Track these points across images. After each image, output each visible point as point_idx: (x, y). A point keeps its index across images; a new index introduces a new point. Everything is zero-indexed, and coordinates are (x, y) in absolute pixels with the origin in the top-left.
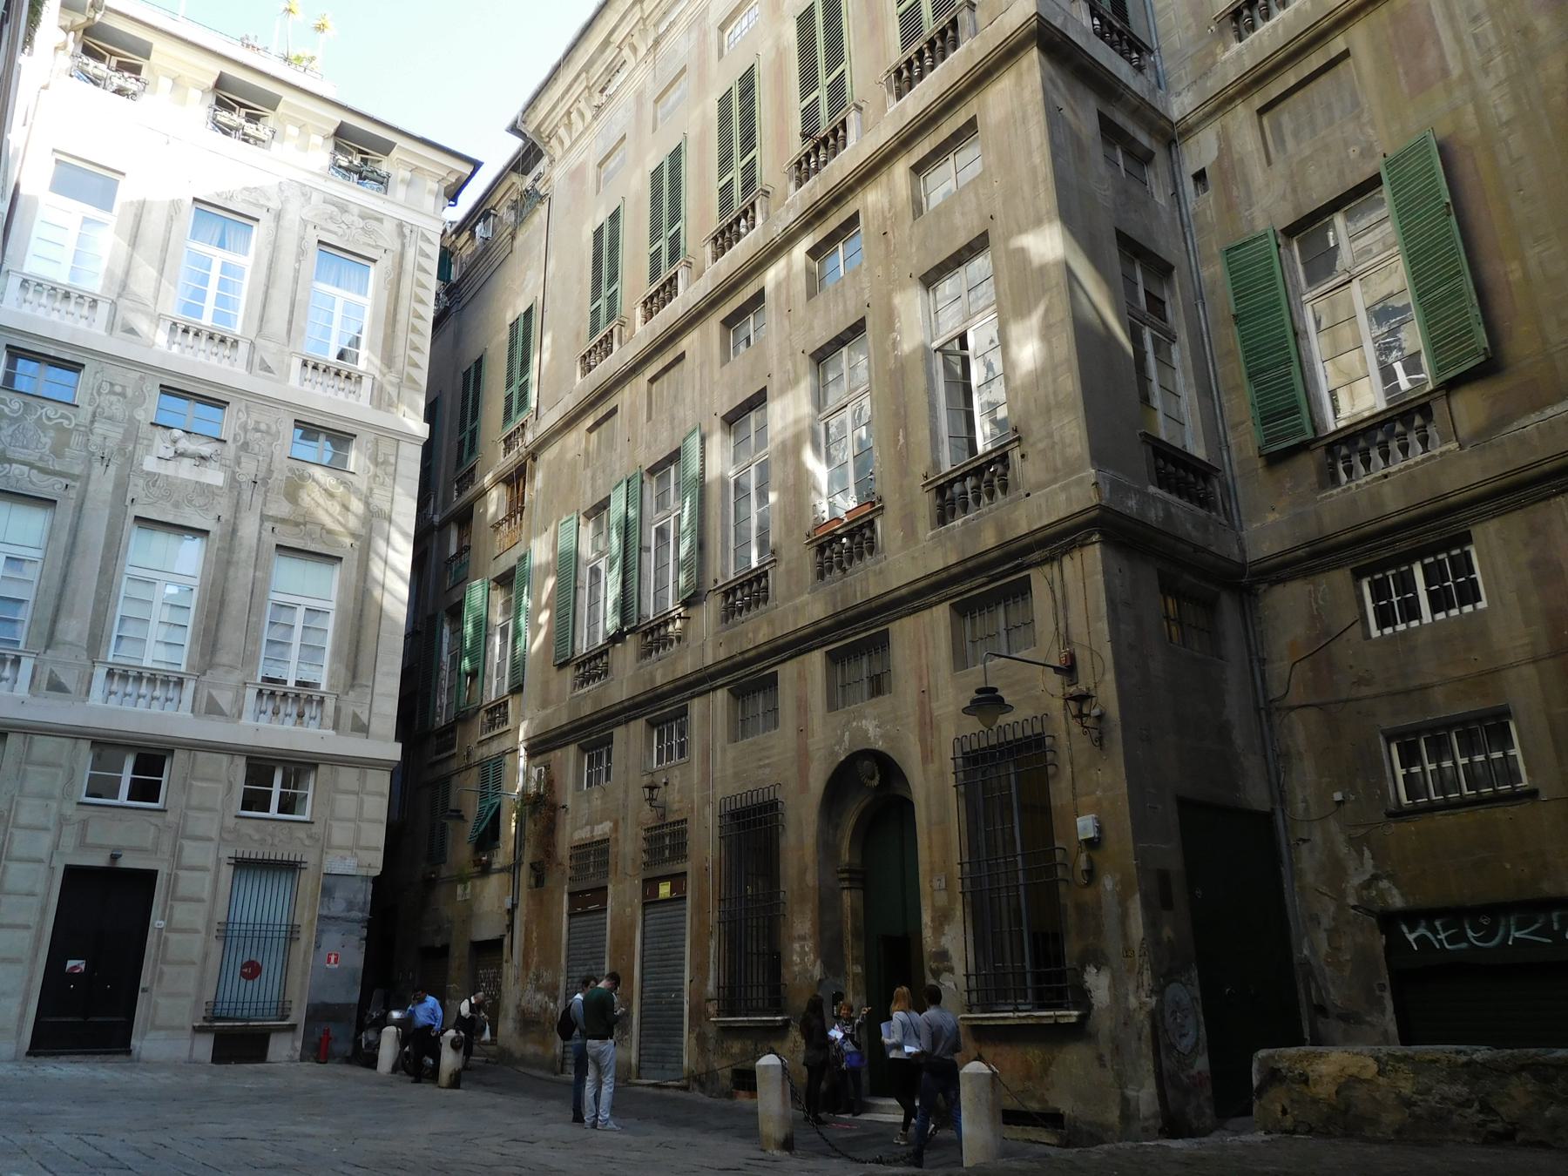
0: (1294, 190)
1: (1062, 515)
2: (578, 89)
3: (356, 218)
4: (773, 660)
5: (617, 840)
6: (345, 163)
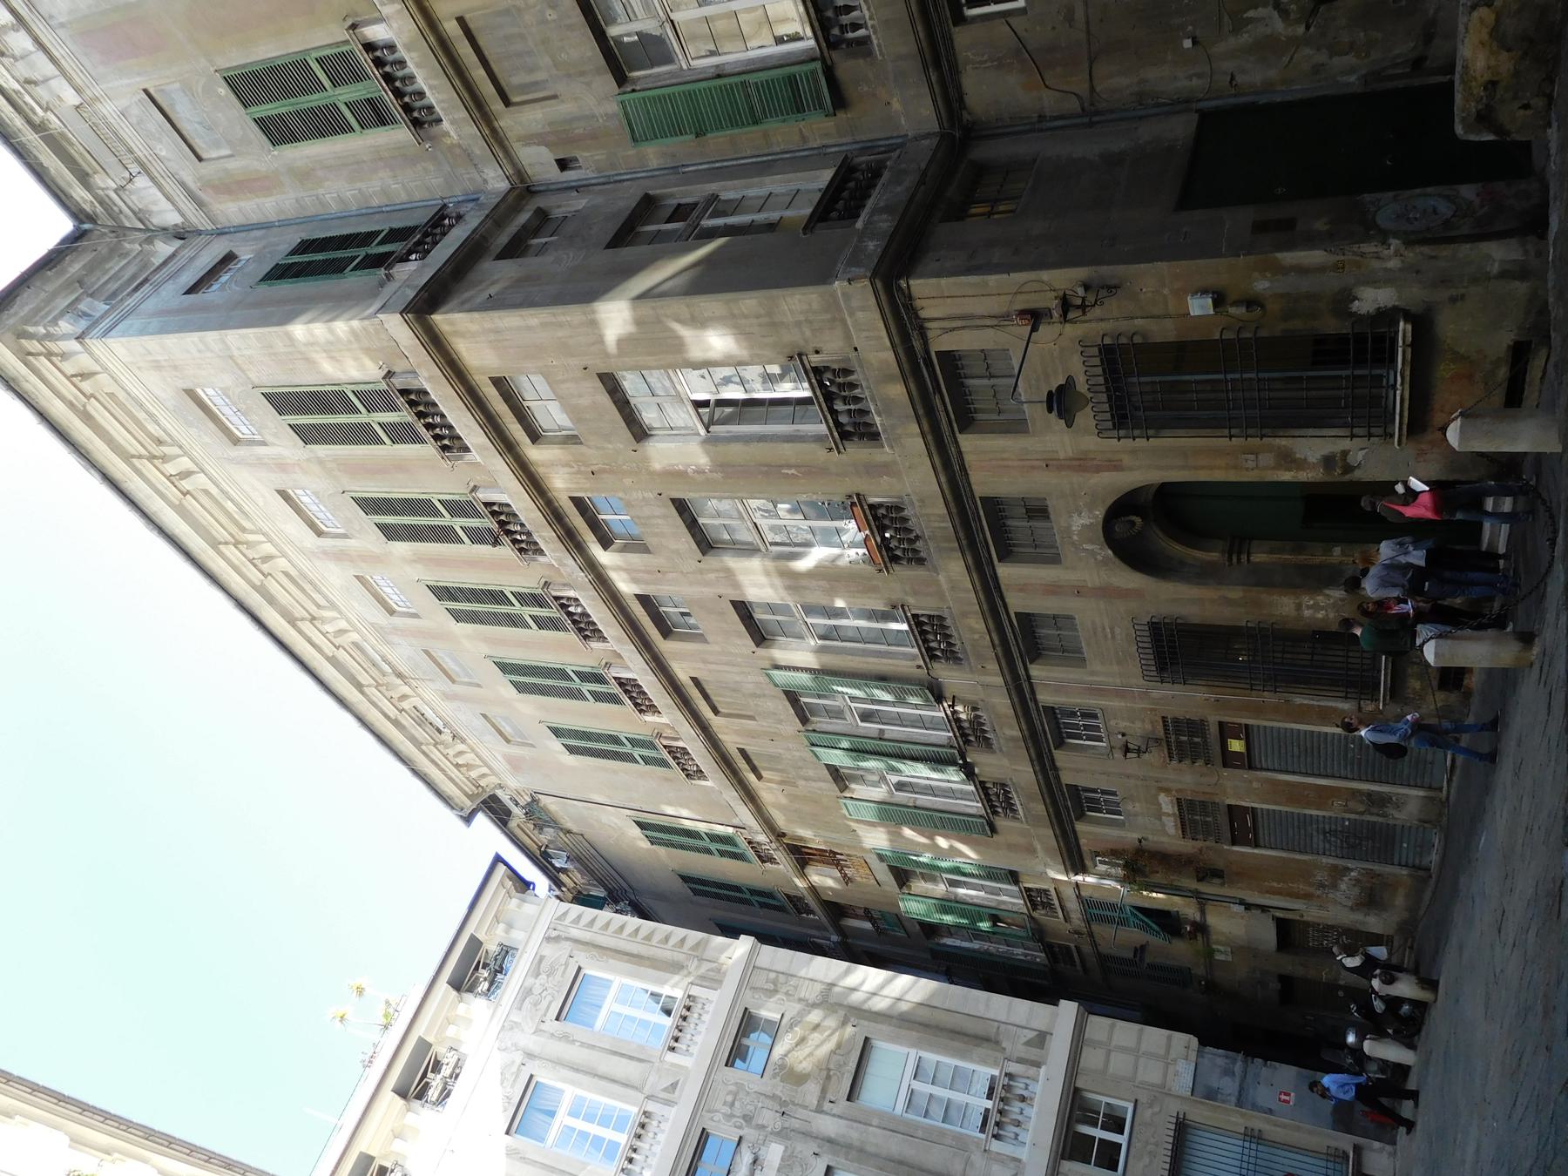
0: (582, 74)
2: (436, 755)
5: (1179, 791)
6: (486, 985)
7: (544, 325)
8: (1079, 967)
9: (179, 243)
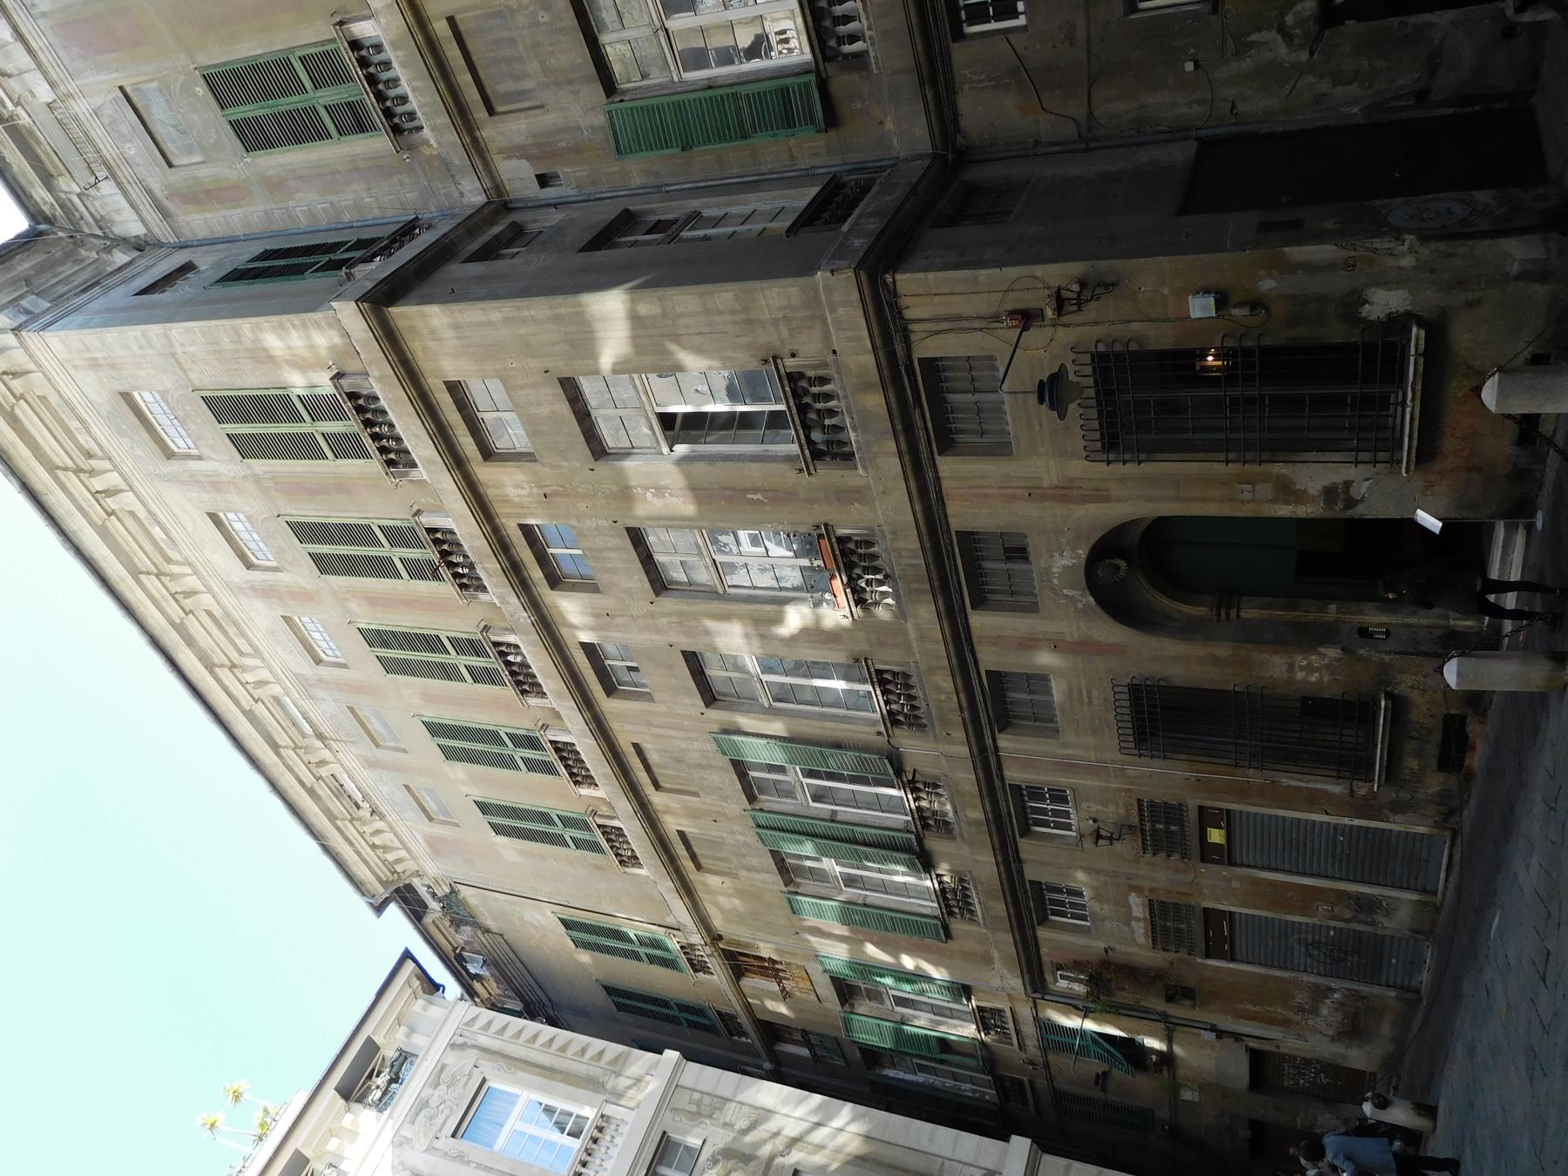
0: (570, 82)
1: (860, 313)
2: (351, 832)
3: (436, 1093)
4: (974, 675)
5: (1152, 890)
6: (378, 1094)
7: (507, 321)
8: (1031, 1107)
9: (136, 254)
